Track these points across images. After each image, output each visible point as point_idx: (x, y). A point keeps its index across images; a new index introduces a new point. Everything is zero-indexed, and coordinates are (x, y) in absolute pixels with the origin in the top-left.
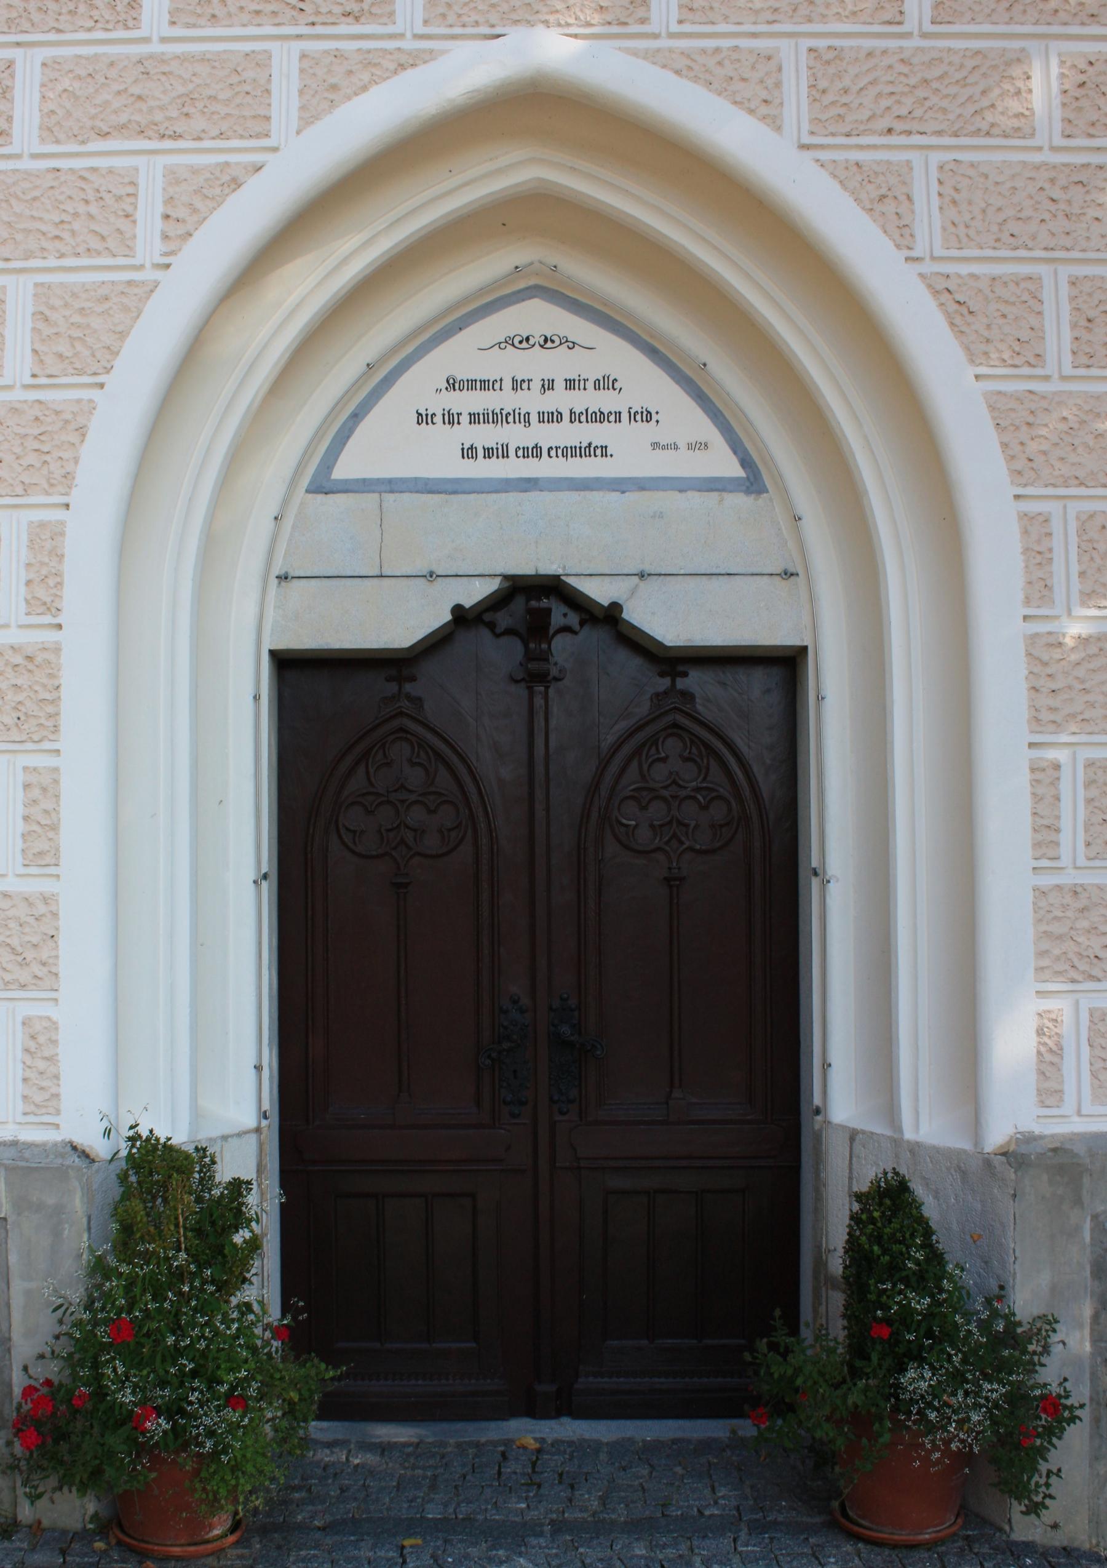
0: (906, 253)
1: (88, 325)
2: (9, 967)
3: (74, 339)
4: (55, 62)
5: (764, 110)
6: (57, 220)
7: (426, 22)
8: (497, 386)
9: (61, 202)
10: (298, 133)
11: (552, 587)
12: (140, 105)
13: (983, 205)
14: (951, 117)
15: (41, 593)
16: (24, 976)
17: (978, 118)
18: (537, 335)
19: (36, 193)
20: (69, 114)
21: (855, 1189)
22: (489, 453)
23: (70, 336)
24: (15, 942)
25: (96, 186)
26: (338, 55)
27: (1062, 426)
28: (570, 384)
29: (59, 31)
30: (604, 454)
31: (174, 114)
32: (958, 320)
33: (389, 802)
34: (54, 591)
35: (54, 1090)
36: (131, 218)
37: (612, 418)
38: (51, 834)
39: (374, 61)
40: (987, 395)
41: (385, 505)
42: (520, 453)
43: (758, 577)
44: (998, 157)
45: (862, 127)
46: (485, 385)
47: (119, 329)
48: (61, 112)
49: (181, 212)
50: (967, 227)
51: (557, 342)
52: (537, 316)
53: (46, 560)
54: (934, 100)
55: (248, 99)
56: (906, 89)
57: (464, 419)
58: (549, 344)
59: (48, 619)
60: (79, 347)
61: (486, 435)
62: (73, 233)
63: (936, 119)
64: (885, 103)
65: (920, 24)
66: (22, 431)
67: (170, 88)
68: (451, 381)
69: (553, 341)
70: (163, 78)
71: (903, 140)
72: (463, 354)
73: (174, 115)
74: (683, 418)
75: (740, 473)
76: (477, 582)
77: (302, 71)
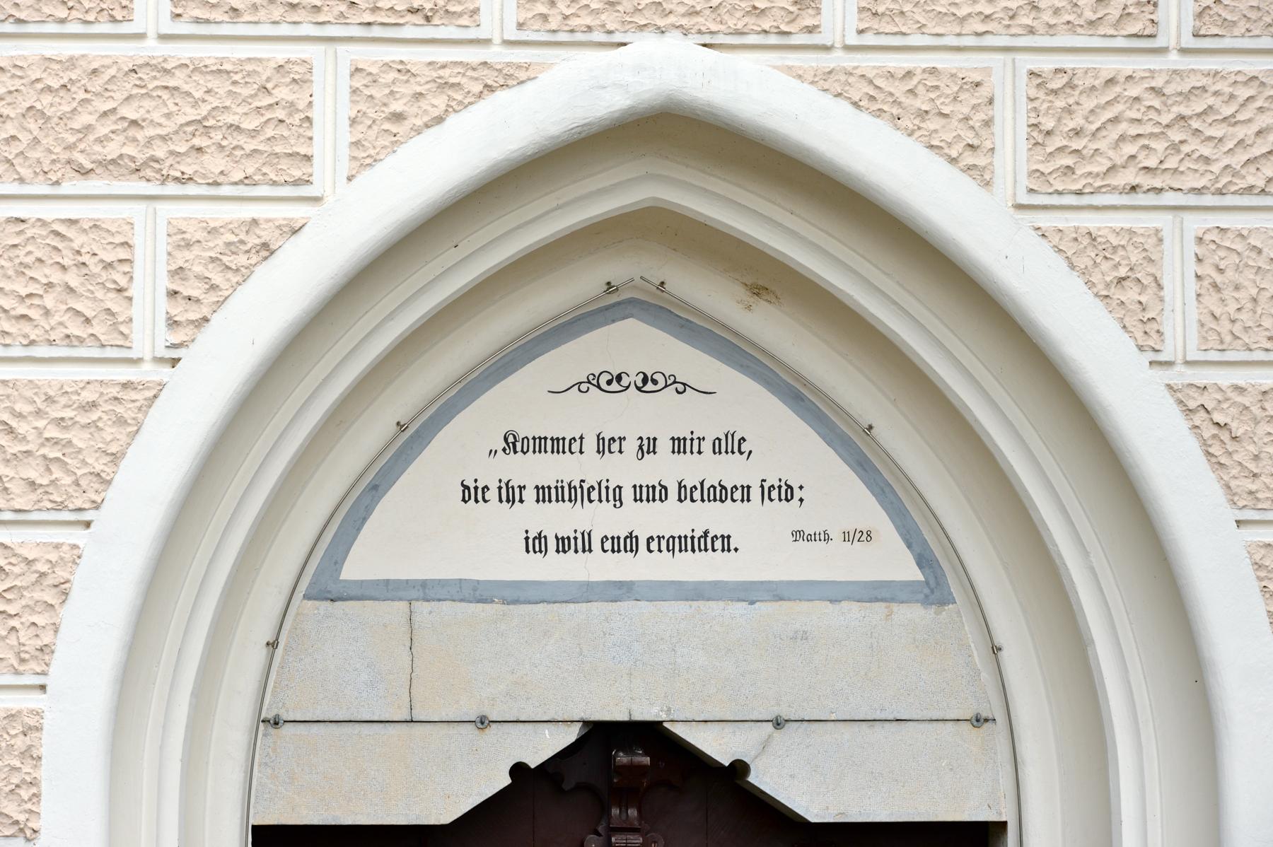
0: (1151, 356)
1: (70, 442)
3: (51, 460)
4: (15, 66)
5: (969, 159)
6: (23, 292)
7: (520, 26)
8: (576, 447)
9: (27, 266)
10: (349, 179)
11: (651, 735)
12: (132, 132)
13: (1254, 291)
14: (1216, 168)
17: (1252, 169)
18: (633, 373)
20: (36, 141)
21: (253, 822)
22: (564, 544)
23: (44, 457)
25: (76, 246)
26: (404, 70)
28: (679, 445)
29: (20, 21)
30: (726, 549)
31: (182, 149)
34: (29, 806)
36: (126, 294)
37: (738, 495)
39: (452, 80)
40: (1249, 548)
41: (416, 618)
42: (608, 545)
43: (940, 724)
45: (1098, 183)
46: (559, 445)
47: (113, 448)
48: (25, 138)
49: (192, 289)
50: (1233, 321)
51: (661, 384)
52: (634, 345)
53: (18, 764)
56: (1157, 130)
57: (530, 495)
58: (650, 386)
60: (57, 473)
61: (560, 519)
62: (47, 313)
63: (1196, 171)
64: (1129, 149)
65: (1179, 36)
67: (175, 108)
68: (511, 439)
69: (655, 382)
70: (165, 95)
71: (1151, 200)
73: (182, 150)
75: (915, 574)
76: (546, 730)
77: (355, 91)
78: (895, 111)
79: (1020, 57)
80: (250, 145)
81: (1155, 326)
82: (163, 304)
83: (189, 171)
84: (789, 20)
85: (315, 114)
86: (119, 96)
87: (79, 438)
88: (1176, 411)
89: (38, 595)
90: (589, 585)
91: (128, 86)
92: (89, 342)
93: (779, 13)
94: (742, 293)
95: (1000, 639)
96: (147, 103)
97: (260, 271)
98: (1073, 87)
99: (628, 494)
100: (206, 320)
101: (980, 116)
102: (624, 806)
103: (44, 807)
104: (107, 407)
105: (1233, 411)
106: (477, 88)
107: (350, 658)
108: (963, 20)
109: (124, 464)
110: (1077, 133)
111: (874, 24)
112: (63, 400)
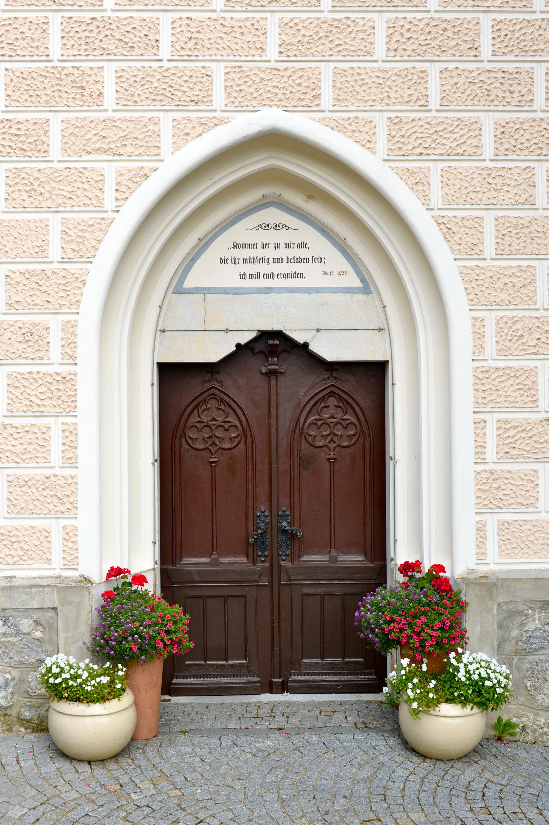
2: (57, 505)
5: (368, 145)
6: (70, 190)
8: (255, 246)
11: (279, 334)
12: (104, 140)
13: (459, 186)
14: (447, 147)
15: (68, 350)
16: (63, 508)
17: (459, 147)
18: (272, 224)
19: (61, 178)
20: (74, 143)
22: (251, 276)
24: (59, 495)
26: (189, 120)
27: (490, 280)
28: (287, 246)
29: (68, 106)
31: (120, 145)
32: (447, 236)
33: (208, 426)
35: (76, 555)
37: (305, 261)
38: (74, 450)
42: (265, 276)
44: (466, 164)
45: (410, 152)
46: (250, 246)
52: (272, 215)
54: (440, 140)
55: (151, 139)
56: (428, 135)
57: (241, 261)
58: (278, 228)
59: (71, 361)
60: (81, 246)
61: (250, 268)
62: (78, 197)
64: (420, 141)
66: (59, 282)
70: (114, 128)
71: (427, 157)
72: (241, 232)
74: (336, 260)
75: (360, 285)
76: (246, 333)
77: (174, 126)
78: (345, 130)
79: (384, 113)
80: (141, 144)
81: (427, 197)
82: (114, 194)
83: (122, 152)
84: (309, 102)
85: (161, 134)
86: (100, 129)
87: (88, 235)
88: (435, 224)
89: (76, 284)
90: (259, 289)
91: (102, 126)
92: (91, 205)
93: (307, 100)
94: (305, 198)
95: (386, 303)
96: (108, 131)
97: (144, 183)
98: (402, 122)
99: (271, 261)
100: (127, 198)
101: (372, 132)
102: (273, 357)
103: (78, 350)
104: (97, 226)
105: (453, 224)
106: (212, 125)
107: (186, 311)
108: (366, 101)
109: (102, 243)
110: (403, 136)
111: (338, 103)
112: (83, 224)
